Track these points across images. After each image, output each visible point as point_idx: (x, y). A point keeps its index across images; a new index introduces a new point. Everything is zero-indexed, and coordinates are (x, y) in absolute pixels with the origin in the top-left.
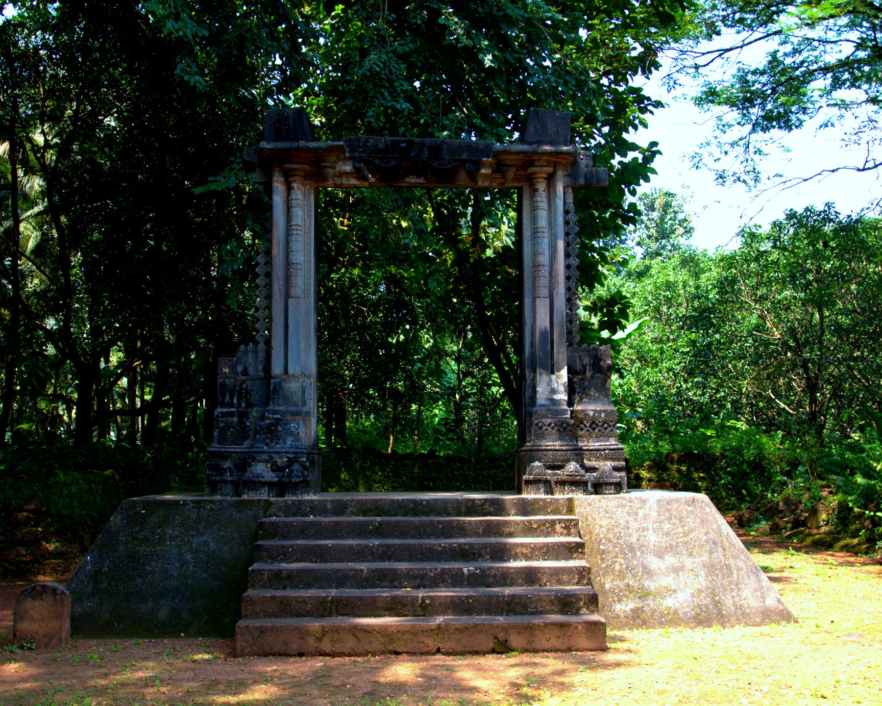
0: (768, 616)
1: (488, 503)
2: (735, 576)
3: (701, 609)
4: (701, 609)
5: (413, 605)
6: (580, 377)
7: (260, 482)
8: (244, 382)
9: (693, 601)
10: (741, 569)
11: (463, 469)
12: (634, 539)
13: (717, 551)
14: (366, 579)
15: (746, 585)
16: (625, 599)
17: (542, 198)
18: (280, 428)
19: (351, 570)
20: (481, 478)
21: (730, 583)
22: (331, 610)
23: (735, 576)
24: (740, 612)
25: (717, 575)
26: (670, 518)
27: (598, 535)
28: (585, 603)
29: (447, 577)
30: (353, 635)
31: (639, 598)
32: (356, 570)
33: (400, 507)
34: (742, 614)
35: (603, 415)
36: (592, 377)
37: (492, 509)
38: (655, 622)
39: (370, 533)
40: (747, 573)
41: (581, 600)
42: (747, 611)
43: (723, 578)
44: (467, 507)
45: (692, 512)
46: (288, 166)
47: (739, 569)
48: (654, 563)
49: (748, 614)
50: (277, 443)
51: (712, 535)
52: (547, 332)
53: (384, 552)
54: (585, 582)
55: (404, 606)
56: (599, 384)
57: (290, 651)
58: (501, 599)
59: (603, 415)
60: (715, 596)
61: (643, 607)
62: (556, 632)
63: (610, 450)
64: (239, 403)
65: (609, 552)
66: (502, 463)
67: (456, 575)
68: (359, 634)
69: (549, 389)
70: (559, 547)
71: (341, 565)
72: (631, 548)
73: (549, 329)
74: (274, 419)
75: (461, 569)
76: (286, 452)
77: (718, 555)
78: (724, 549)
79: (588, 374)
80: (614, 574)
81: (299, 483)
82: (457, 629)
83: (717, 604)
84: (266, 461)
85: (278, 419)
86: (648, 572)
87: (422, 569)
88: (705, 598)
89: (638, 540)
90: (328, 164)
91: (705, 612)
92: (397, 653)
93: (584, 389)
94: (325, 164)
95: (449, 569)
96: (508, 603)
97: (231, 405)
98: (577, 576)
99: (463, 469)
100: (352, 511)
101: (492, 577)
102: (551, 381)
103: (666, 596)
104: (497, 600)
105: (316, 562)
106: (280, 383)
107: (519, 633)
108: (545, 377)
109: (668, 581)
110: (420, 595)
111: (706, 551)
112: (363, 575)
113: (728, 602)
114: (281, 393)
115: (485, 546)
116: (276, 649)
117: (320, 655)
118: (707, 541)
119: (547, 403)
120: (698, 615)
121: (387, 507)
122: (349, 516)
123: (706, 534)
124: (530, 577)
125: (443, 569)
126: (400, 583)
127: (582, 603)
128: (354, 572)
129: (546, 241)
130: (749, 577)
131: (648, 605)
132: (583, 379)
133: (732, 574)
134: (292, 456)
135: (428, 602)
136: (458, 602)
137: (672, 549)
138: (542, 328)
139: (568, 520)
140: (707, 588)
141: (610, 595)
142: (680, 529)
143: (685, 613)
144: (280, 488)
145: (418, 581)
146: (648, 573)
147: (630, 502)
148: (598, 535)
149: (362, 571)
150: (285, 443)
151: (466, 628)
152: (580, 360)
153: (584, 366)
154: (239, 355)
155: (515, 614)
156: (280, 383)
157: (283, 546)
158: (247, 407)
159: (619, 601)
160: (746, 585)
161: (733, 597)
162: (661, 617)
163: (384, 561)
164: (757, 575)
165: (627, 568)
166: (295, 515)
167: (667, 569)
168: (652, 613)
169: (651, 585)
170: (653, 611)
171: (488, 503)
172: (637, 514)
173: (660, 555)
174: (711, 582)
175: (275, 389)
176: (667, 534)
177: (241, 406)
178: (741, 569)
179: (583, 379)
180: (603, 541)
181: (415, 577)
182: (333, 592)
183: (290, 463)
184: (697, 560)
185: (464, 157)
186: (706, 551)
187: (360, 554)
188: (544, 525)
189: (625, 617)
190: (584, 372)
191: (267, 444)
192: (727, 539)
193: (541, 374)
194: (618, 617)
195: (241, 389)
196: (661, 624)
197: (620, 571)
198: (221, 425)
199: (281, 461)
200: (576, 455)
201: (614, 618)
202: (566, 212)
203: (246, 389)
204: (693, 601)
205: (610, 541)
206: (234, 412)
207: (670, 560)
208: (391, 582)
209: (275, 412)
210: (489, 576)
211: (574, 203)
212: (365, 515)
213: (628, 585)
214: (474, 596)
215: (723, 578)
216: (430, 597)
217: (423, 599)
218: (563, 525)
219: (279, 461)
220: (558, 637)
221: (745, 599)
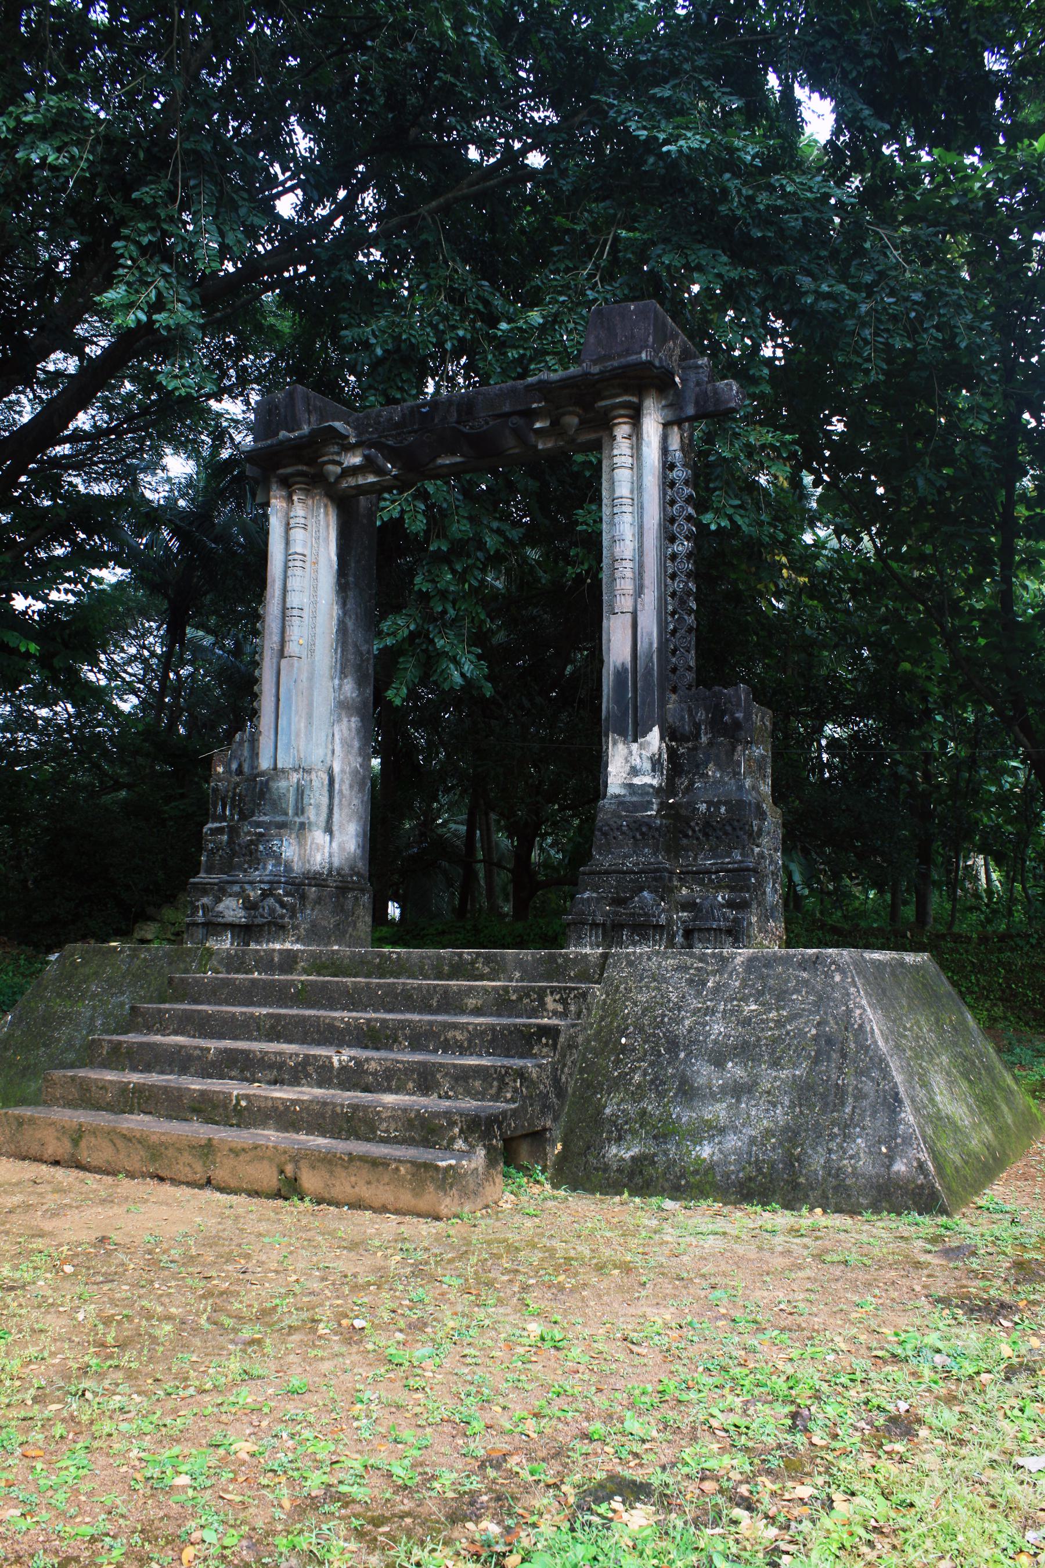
0: (888, 1196)
1: (481, 960)
2: (848, 1110)
3: (759, 1170)
4: (759, 1170)
5: (225, 1107)
6: (690, 745)
7: (219, 924)
8: (237, 784)
9: (749, 1153)
10: (865, 1096)
11: (957, 951)
12: (682, 1030)
13: (829, 1060)
14: (213, 1064)
15: (863, 1128)
16: (629, 1137)
17: (622, 447)
18: (261, 848)
19: (196, 1048)
20: (987, 965)
21: (834, 1123)
22: (132, 1105)
23: (848, 1110)
24: (834, 1182)
25: (813, 1106)
26: (761, 993)
27: (625, 1018)
28: (461, 1131)
29: (310, 1069)
30: (111, 1140)
31: (655, 1137)
32: (202, 1049)
33: (362, 963)
34: (836, 1188)
35: (723, 810)
36: (711, 744)
37: (487, 970)
38: (666, 1185)
39: (291, 999)
40: (873, 1106)
41: (455, 1123)
42: (848, 1182)
43: (823, 1111)
44: (451, 965)
45: (806, 983)
46: (281, 471)
47: (860, 1096)
48: (704, 1073)
49: (847, 1188)
50: (257, 869)
51: (831, 1027)
52: (625, 670)
53: (272, 1027)
54: (509, 1095)
55: (215, 1107)
56: (723, 757)
57: (46, 1157)
58: (338, 1109)
59: (723, 810)
60: (795, 1147)
61: (655, 1155)
62: (365, 1172)
63: (727, 871)
64: (232, 815)
65: (634, 1050)
66: (1021, 943)
67: (323, 1067)
68: (118, 1142)
69: (628, 769)
70: (511, 1033)
71: (158, 1038)
72: (673, 1045)
73: (629, 667)
74: (256, 834)
75: (329, 1058)
76: (261, 882)
77: (829, 1069)
78: (844, 1056)
79: (704, 739)
80: (626, 1090)
81: (263, 925)
82: (231, 1150)
83: (790, 1161)
84: (237, 895)
85: (261, 835)
86: (688, 1092)
87: (280, 1054)
88: (774, 1149)
89: (690, 1031)
90: (325, 459)
91: (765, 1176)
92: (162, 1179)
93: (697, 766)
94: (325, 459)
95: (314, 1056)
96: (349, 1119)
97: (223, 818)
98: (495, 1083)
99: (957, 951)
100: (303, 968)
101: (371, 1074)
102: (631, 753)
103: (702, 1138)
104: (333, 1111)
105: (194, 1037)
106: (267, 781)
107: (314, 1168)
108: (621, 746)
109: (718, 1111)
110: (235, 1093)
111: (809, 1057)
112: (210, 1057)
113: (817, 1161)
114: (267, 796)
115: (402, 1024)
116: (32, 1152)
117: (77, 1167)
118: (816, 1038)
119: (623, 792)
120: (750, 1179)
121: (346, 961)
122: (299, 974)
123: (819, 1024)
124: (426, 1079)
125: (307, 1056)
126: (253, 1074)
127: (457, 1130)
128: (198, 1052)
129: (627, 518)
130: (873, 1115)
131: (666, 1153)
132: (695, 749)
133: (843, 1104)
134: (266, 887)
135: (243, 1103)
136: (281, 1108)
137: (744, 1051)
138: (619, 664)
139: (565, 988)
140: (787, 1128)
141: (607, 1127)
142: (773, 1015)
143: (727, 1175)
144: (245, 932)
145: (275, 1072)
146: (685, 1093)
147: (701, 960)
148: (625, 1018)
149: (208, 1050)
150: (265, 868)
151: (243, 1150)
152: (691, 715)
153: (697, 726)
154: (234, 746)
155: (358, 1138)
156: (267, 781)
157: (160, 1010)
158: (239, 820)
159: (620, 1139)
160: (863, 1128)
161: (830, 1151)
162: (679, 1178)
163: (271, 1040)
164: (894, 1111)
165: (652, 1082)
166: (237, 972)
167: (723, 1089)
168: (668, 1168)
169: (684, 1115)
170: (671, 1164)
171: (481, 960)
172: (704, 983)
173: (718, 1062)
174: (795, 1118)
175: (261, 790)
176: (746, 1022)
177: (233, 819)
178: (865, 1096)
179: (695, 749)
180: (631, 1029)
181: (271, 1066)
182: (135, 1078)
183: (265, 895)
184: (784, 1074)
185: (507, 408)
186: (809, 1057)
187: (276, 1031)
188: (528, 996)
189: (618, 1170)
190: (697, 736)
191: (245, 871)
192: (856, 1036)
193: (615, 743)
194: (606, 1168)
195: (235, 795)
196: (676, 1192)
197: (639, 1086)
198: (211, 846)
199: (254, 894)
200: (655, 879)
201: (596, 1169)
202: (668, 466)
203: (240, 795)
204: (749, 1153)
205: (641, 1030)
206: (223, 828)
207: (735, 1070)
208: (242, 1071)
209: (259, 825)
210: (366, 1072)
211: (682, 449)
212: (319, 974)
213: (643, 1112)
214: (303, 1101)
215: (823, 1111)
216: (247, 1097)
217: (238, 1098)
218: (558, 997)
219: (252, 894)
220: (369, 1183)
221: (851, 1157)
